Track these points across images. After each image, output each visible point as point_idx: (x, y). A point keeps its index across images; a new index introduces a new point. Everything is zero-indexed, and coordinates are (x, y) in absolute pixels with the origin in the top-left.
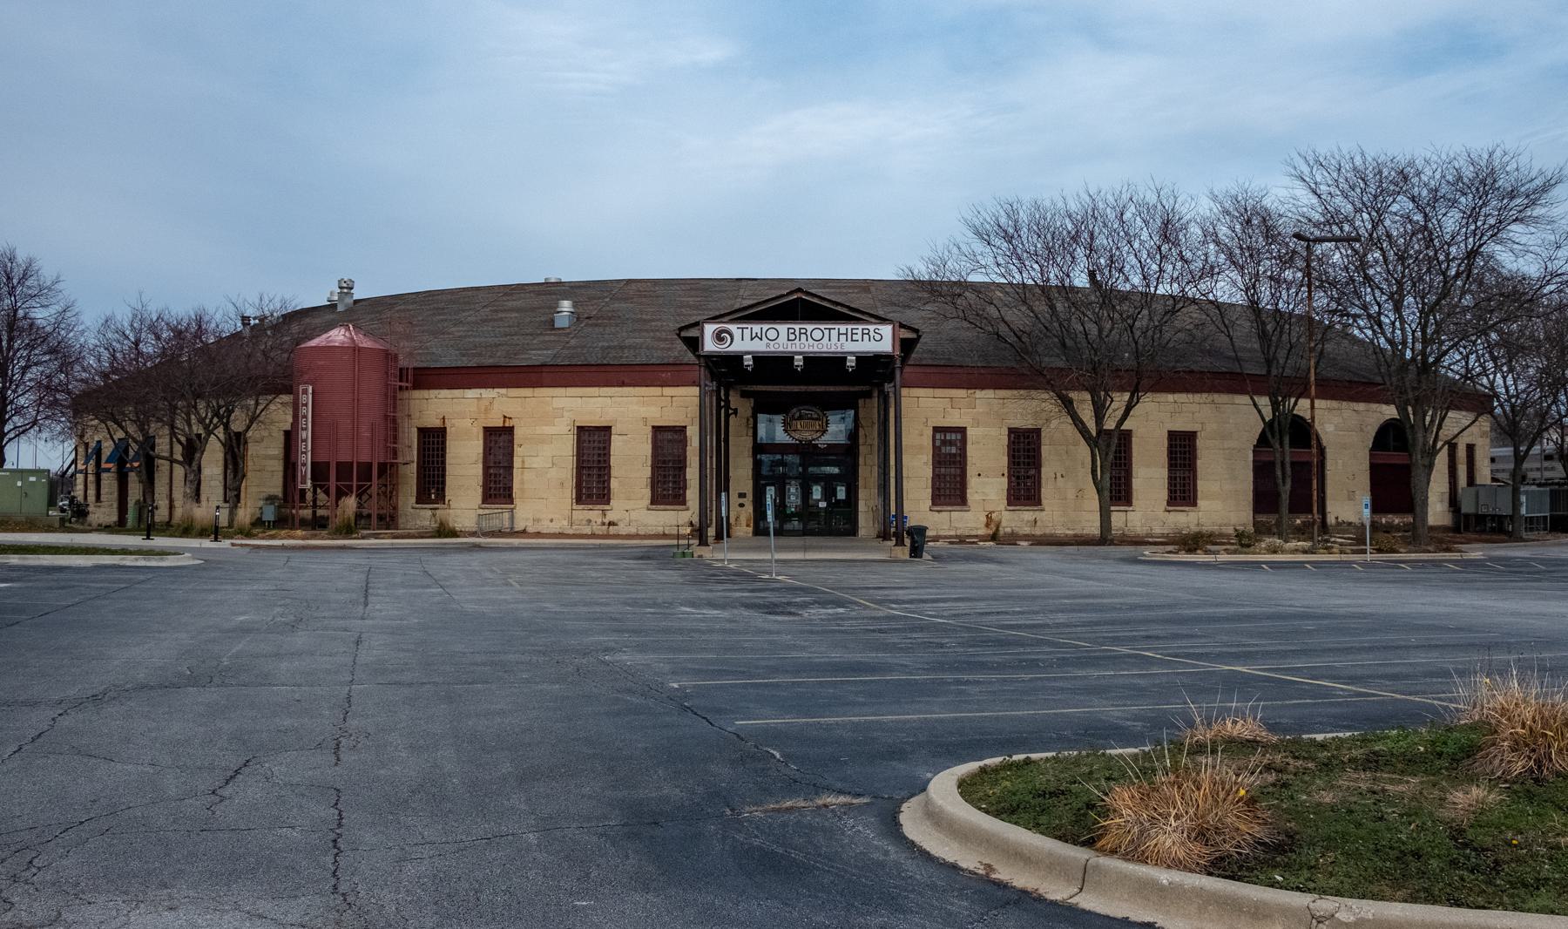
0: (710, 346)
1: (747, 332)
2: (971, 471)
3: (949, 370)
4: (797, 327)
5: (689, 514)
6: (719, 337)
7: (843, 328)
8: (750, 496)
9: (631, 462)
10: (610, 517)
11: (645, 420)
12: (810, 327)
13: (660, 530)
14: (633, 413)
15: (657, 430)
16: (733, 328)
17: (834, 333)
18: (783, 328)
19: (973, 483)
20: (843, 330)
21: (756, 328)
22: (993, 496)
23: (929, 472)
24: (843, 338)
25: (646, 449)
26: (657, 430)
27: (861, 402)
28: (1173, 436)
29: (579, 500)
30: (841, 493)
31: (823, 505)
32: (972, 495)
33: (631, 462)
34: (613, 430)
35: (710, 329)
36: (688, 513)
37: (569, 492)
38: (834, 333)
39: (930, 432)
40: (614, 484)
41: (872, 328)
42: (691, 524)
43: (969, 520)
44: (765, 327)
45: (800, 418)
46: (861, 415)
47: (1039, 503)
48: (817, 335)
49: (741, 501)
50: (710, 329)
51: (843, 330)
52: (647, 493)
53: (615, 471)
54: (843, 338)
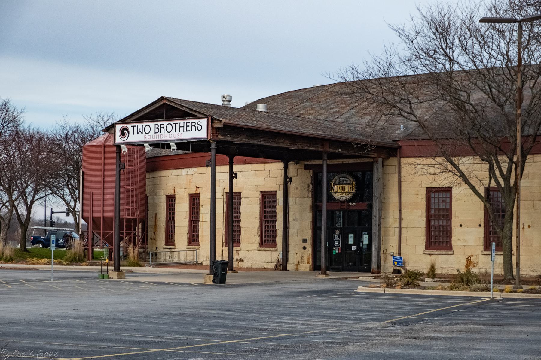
2: (455, 223)
4: (159, 123)
5: (276, 255)
7: (182, 122)
8: (310, 242)
12: (165, 123)
14: (257, 178)
16: (129, 126)
18: (152, 124)
19: (456, 231)
21: (140, 125)
22: (471, 243)
23: (422, 223)
31: (354, 248)
32: (455, 242)
36: (276, 254)
39: (423, 192)
41: (196, 121)
43: (449, 263)
45: (339, 183)
47: (451, 248)
48: (169, 128)
49: (305, 244)
52: (257, 239)
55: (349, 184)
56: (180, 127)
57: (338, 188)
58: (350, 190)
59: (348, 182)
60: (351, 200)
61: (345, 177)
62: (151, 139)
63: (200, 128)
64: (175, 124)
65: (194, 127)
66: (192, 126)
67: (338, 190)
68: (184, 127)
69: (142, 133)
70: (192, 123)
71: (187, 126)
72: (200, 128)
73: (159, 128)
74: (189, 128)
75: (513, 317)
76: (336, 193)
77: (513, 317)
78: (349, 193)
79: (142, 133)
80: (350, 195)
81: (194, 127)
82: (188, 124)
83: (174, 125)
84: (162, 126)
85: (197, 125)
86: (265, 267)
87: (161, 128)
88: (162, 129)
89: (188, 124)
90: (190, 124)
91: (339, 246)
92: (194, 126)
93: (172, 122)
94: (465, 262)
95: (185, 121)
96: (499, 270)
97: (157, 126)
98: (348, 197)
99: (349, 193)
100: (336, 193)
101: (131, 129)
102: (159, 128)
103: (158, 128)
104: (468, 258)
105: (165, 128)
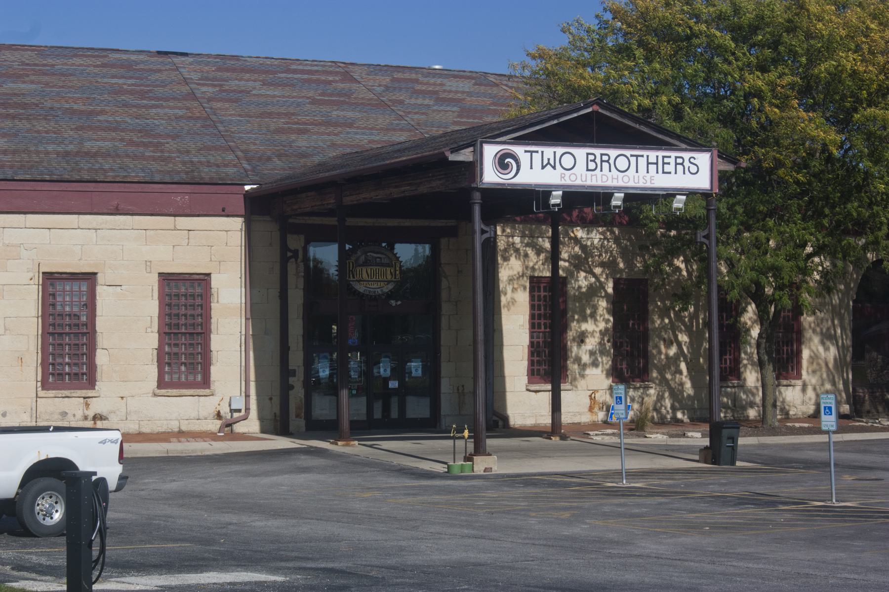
0: (490, 175)
1: (537, 157)
3: (91, 187)
4: (598, 152)
6: (502, 163)
7: (653, 155)
9: (128, 327)
10: (96, 406)
11: (148, 263)
12: (613, 153)
13: (174, 426)
15: (166, 279)
16: (519, 150)
17: (642, 162)
18: (580, 153)
20: (652, 159)
21: (549, 152)
24: (652, 168)
25: (152, 308)
26: (166, 279)
27: (444, 241)
28: (51, 280)
29: (45, 385)
30: (415, 367)
33: (128, 327)
34: (100, 278)
35: (490, 151)
37: (32, 371)
38: (642, 162)
40: (101, 358)
41: (686, 155)
42: (219, 416)
44: (560, 150)
45: (366, 263)
46: (445, 258)
48: (622, 163)
50: (490, 151)
51: (652, 159)
52: (152, 371)
53: (104, 339)
54: (652, 168)
55: (388, 265)
56: (648, 163)
57: (364, 273)
58: (389, 277)
59: (386, 261)
60: (390, 295)
61: (377, 253)
62: (631, 184)
63: (693, 169)
64: (637, 156)
65: (680, 168)
66: (676, 164)
67: (365, 276)
68: (657, 164)
69: (554, 167)
70: (676, 158)
71: (664, 163)
72: (693, 169)
73: (598, 160)
74: (667, 168)
75: (870, 469)
76: (359, 281)
77: (870, 469)
78: (389, 282)
79: (554, 167)
80: (391, 286)
81: (680, 168)
82: (666, 160)
83: (633, 160)
84: (605, 158)
85: (687, 164)
86: (184, 428)
87: (602, 161)
88: (605, 165)
89: (666, 160)
90: (672, 161)
91: (360, 382)
92: (682, 164)
93: (628, 153)
94: (588, 401)
95: (661, 154)
96: (546, 420)
97: (591, 157)
98: (386, 290)
99: (389, 282)
100: (359, 281)
101: (524, 158)
102: (598, 160)
103: (594, 161)
104: (590, 396)
105: (612, 161)
